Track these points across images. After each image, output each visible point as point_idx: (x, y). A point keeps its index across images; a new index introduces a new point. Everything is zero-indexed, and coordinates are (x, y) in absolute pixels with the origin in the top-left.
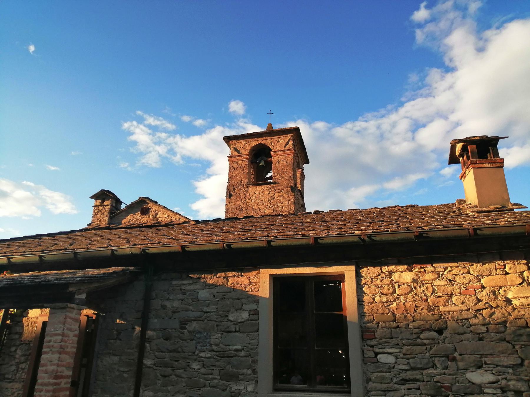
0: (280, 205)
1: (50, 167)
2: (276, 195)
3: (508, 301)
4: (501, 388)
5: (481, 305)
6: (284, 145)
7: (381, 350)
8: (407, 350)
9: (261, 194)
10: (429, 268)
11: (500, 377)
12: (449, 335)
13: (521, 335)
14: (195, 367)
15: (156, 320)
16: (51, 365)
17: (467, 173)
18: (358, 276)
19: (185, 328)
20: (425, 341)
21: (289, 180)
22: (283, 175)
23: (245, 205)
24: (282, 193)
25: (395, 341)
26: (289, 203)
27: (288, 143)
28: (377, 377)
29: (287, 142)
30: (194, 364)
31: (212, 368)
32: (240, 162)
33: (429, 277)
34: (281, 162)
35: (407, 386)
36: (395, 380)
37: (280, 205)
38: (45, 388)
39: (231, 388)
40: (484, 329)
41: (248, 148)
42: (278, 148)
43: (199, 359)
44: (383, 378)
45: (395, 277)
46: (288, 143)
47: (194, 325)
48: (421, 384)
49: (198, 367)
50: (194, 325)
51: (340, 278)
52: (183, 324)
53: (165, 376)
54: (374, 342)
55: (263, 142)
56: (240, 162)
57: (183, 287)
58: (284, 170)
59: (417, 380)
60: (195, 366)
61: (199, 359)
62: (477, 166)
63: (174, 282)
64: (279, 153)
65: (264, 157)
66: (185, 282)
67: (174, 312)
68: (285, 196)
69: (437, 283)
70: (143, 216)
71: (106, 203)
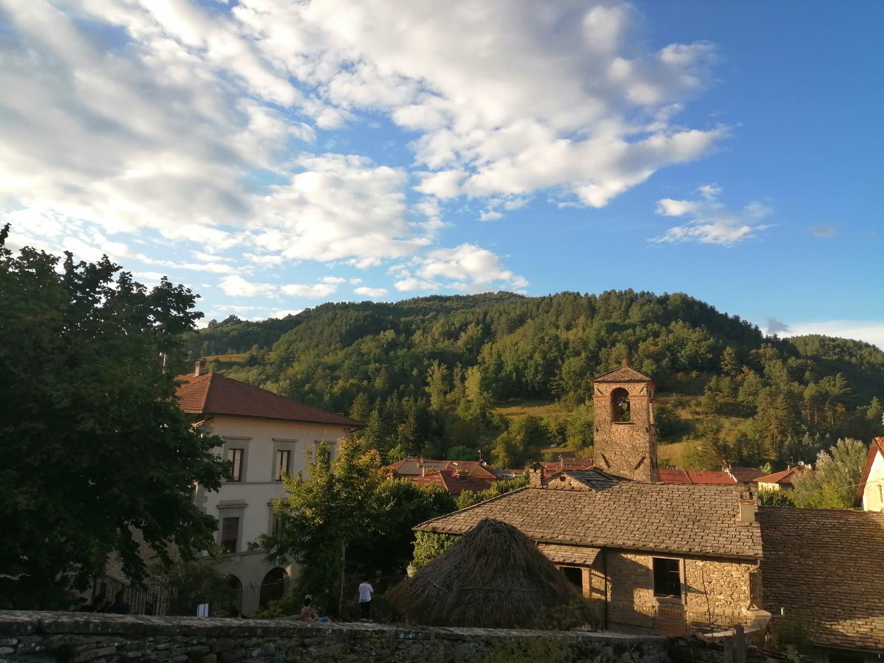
1: (623, 555)
2: (634, 433)
3: (732, 575)
5: (723, 576)
9: (622, 431)
10: (708, 562)
18: (684, 562)
22: (639, 417)
23: (610, 439)
24: (639, 433)
27: (642, 389)
32: (603, 402)
33: (708, 564)
34: (637, 406)
41: (610, 390)
45: (697, 563)
46: (642, 389)
47: (452, 455)
50: (452, 455)
51: (679, 561)
52: (620, 571)
55: (622, 387)
56: (603, 402)
58: (640, 413)
60: (627, 586)
68: (642, 435)
69: (710, 567)
71: (537, 471)
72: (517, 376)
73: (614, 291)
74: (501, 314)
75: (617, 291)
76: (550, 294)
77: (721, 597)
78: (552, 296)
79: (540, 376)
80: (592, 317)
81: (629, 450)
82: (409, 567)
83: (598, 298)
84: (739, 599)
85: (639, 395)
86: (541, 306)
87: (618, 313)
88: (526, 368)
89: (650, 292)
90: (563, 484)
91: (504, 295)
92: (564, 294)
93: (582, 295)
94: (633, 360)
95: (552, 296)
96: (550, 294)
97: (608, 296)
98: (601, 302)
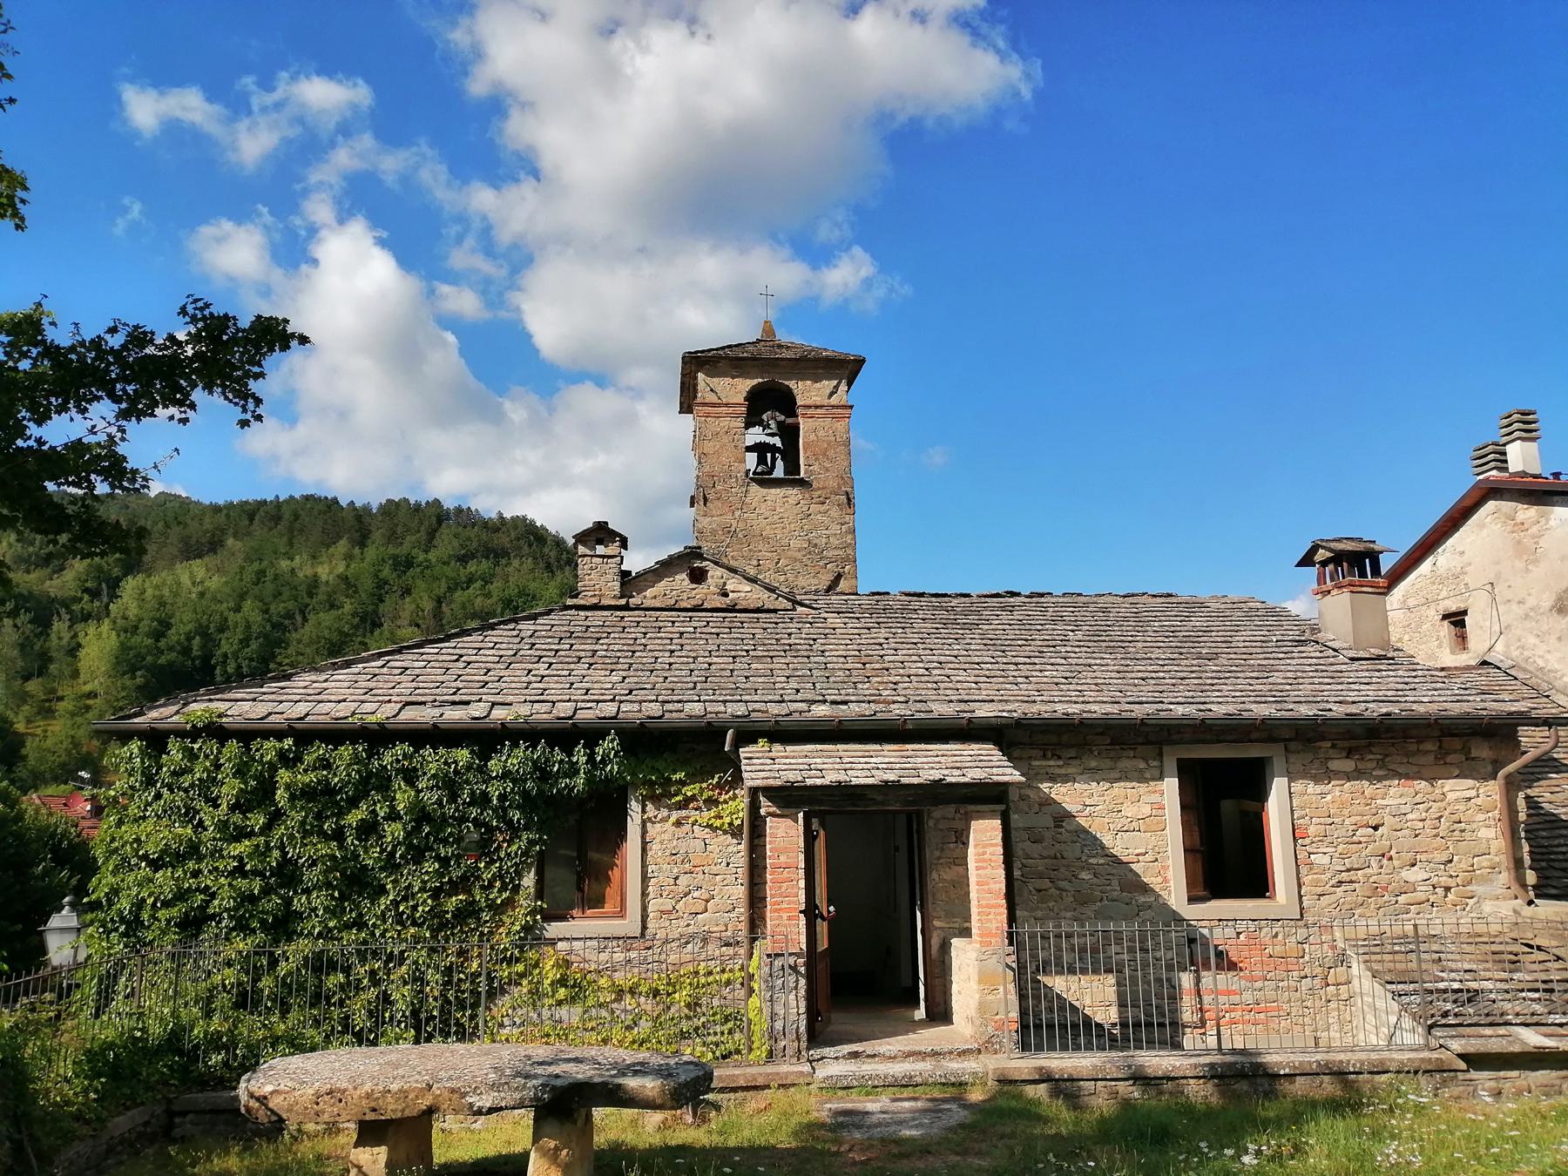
0: (824, 532)
4: (1433, 886)
6: (828, 392)
7: (1315, 850)
8: (1344, 849)
11: (1432, 875)
12: (1385, 832)
13: (1454, 831)
14: (1086, 878)
15: (1016, 816)
16: (995, 883)
17: (1333, 593)
19: (1062, 827)
20: (1361, 839)
21: (843, 478)
25: (1329, 839)
26: (844, 530)
28: (1313, 880)
29: (835, 387)
30: (1083, 873)
31: (1108, 877)
35: (1343, 888)
36: (1331, 883)
37: (824, 532)
38: (993, 910)
39: (1136, 901)
40: (1421, 824)
42: (814, 398)
43: (1088, 867)
44: (1319, 881)
48: (1357, 885)
49: (1089, 877)
53: (1040, 891)
54: (1307, 841)
57: (1051, 770)
58: (831, 453)
59: (1351, 882)
60: (1085, 875)
61: (1088, 867)
62: (1356, 589)
63: (1034, 763)
64: (819, 411)
65: (777, 414)
66: (1051, 763)
67: (1040, 805)
70: (694, 586)
72: (203, 647)
73: (406, 500)
74: (167, 526)
75: (412, 502)
76: (277, 497)
77: (1414, 875)
78: (281, 500)
79: (254, 645)
80: (362, 544)
81: (799, 555)
82: (55, 921)
83: (374, 511)
84: (1471, 876)
85: (826, 402)
86: (257, 518)
87: (414, 538)
88: (222, 629)
89: (473, 509)
90: (700, 593)
91: (170, 501)
92: (307, 498)
93: (344, 503)
94: (444, 622)
95: (281, 500)
96: (277, 497)
97: (392, 509)
98: (380, 518)
